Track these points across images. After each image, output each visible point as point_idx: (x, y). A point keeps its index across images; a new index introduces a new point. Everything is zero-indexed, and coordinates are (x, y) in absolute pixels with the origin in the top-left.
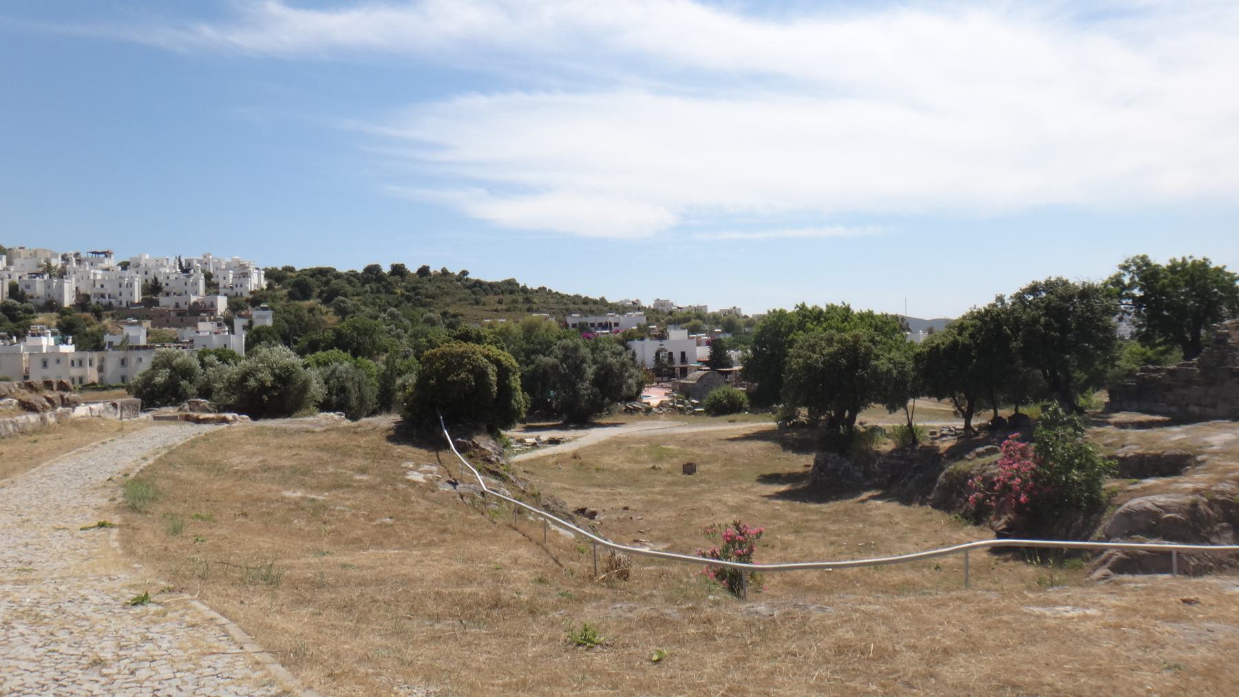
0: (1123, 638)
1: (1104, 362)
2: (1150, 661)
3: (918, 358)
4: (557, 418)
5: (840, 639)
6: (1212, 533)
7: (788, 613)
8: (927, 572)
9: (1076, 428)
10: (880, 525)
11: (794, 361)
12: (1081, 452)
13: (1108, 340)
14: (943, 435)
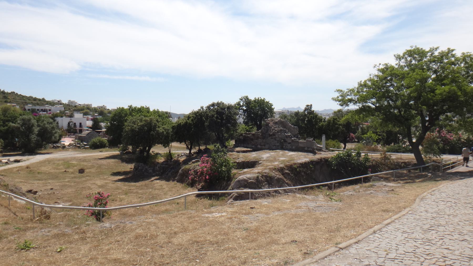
0: (232, 222)
1: (234, 131)
2: (240, 228)
3: (173, 128)
4: (19, 151)
5: (137, 233)
6: (262, 186)
7: (117, 226)
8: (174, 205)
9: (224, 153)
10: (158, 189)
11: (127, 128)
12: (227, 161)
13: (235, 124)
14: (182, 156)
